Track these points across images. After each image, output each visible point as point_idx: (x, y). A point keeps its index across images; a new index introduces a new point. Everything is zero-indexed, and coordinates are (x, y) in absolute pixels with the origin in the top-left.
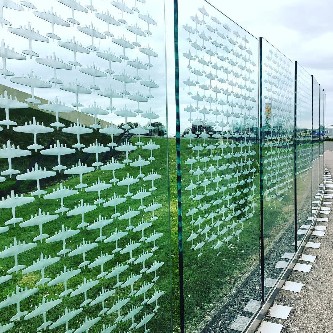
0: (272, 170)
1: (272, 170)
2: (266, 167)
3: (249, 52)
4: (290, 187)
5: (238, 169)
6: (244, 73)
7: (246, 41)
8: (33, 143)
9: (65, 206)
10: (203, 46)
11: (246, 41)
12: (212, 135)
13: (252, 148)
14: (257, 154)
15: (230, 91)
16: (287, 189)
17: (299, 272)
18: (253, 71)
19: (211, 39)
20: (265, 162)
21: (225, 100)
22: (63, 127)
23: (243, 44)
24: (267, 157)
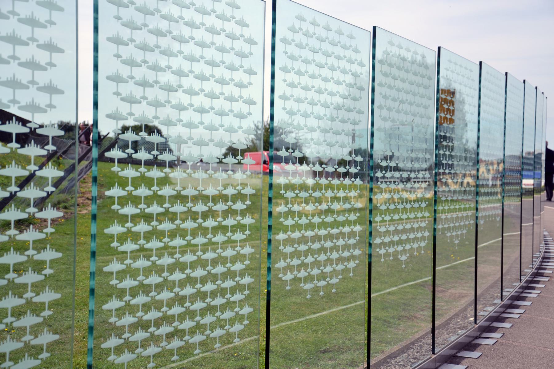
0: (387, 232)
1: (387, 232)
2: (378, 250)
3: (357, 51)
4: (423, 244)
5: (331, 188)
6: (349, 54)
7: (351, 37)
8: (12, 142)
9: (34, 249)
10: (299, 110)
11: (351, 37)
12: (298, 194)
13: (355, 246)
14: (364, 160)
15: (323, 62)
16: (415, 246)
17: (532, 298)
18: (361, 98)
19: (302, 30)
20: (375, 242)
21: (317, 74)
22: (132, 227)
23: (348, 42)
24: (380, 235)
